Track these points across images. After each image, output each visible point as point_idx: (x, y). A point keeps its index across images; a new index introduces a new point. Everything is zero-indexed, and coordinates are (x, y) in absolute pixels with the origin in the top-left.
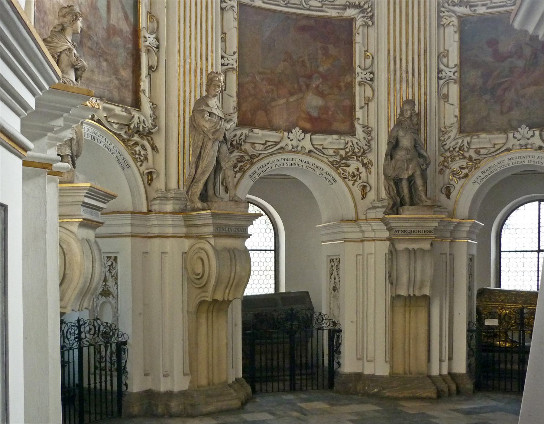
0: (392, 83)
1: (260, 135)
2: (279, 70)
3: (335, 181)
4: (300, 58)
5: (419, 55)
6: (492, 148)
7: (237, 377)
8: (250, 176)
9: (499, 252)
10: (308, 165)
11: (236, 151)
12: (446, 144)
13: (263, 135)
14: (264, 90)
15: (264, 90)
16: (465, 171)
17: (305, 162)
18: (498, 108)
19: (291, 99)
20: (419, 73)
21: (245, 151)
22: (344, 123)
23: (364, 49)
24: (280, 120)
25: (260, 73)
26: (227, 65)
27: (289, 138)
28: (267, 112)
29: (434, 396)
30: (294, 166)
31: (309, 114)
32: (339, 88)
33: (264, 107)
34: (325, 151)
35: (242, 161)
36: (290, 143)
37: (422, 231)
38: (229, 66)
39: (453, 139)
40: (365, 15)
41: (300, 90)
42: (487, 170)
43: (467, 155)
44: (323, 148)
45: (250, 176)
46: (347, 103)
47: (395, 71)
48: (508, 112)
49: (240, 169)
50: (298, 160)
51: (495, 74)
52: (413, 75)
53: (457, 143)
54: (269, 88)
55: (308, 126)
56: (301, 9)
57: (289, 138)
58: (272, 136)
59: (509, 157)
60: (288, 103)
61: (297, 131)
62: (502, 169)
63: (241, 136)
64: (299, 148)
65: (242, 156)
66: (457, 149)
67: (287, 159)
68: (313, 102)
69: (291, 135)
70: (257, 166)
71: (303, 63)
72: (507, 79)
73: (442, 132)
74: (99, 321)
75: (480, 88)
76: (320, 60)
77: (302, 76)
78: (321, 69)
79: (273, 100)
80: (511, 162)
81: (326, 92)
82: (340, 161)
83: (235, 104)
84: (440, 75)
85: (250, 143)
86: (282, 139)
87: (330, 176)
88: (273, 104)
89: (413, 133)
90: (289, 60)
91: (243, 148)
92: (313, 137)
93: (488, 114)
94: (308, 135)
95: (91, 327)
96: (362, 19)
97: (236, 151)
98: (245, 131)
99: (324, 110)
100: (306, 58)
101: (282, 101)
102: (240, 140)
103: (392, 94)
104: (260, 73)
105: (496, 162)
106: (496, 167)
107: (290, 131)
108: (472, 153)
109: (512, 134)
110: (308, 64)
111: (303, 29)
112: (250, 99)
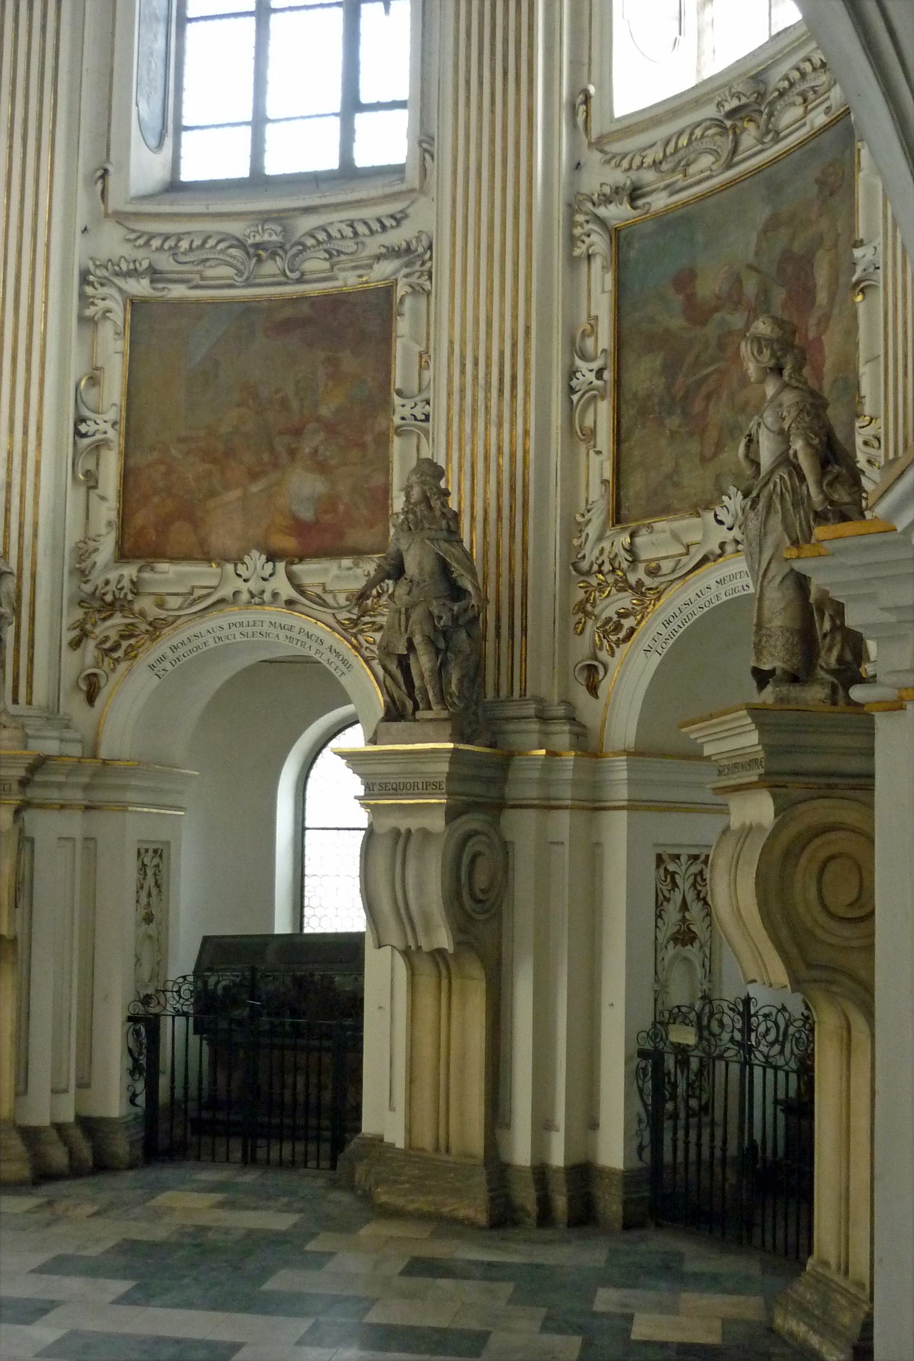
0: (456, 419)
1: (171, 575)
2: (224, 429)
3: (349, 666)
4: (277, 392)
5: (514, 345)
6: (682, 555)
7: (85, 1113)
8: (152, 667)
9: (300, 829)
10: (289, 634)
11: (118, 614)
12: (584, 557)
13: (181, 577)
14: (190, 476)
15: (190, 476)
16: (627, 623)
17: (282, 627)
18: (694, 447)
19: (254, 488)
20: (514, 386)
21: (142, 614)
22: (371, 527)
23: (417, 349)
24: (222, 538)
25: (181, 440)
26: (94, 435)
27: (239, 575)
28: (195, 524)
29: (482, 1218)
30: (258, 638)
31: (295, 518)
32: (363, 446)
33: (190, 513)
34: (329, 598)
35: (131, 636)
36: (244, 587)
37: (420, 786)
38: (99, 436)
39: (602, 544)
40: (417, 267)
41: (275, 465)
42: (674, 616)
43: (632, 579)
44: (325, 591)
45: (152, 667)
46: (377, 480)
47: (462, 390)
48: (715, 455)
49: (126, 653)
50: (266, 625)
51: (690, 358)
52: (501, 391)
53: (602, 551)
54: (201, 469)
55: (289, 543)
56: (285, 284)
57: (239, 575)
58: (201, 574)
59: (717, 576)
60: (245, 498)
61: (256, 560)
62: (706, 609)
63: (119, 582)
64: (267, 596)
65: (132, 624)
66: (607, 567)
67: (241, 624)
68: (303, 488)
69: (241, 569)
70: (169, 644)
71: (284, 404)
72: (712, 368)
73: (573, 528)
74: (787, 1015)
75: (661, 402)
76: (321, 389)
77: (281, 433)
78: (325, 411)
79: (212, 494)
80: (722, 589)
81: (333, 462)
82: (358, 619)
83: (113, 515)
84: (574, 383)
85: (154, 594)
86: (223, 578)
87: (338, 654)
88: (211, 504)
89: (431, 540)
90: (251, 401)
91: (136, 607)
92: (296, 568)
93: (677, 464)
94: (281, 566)
95: (770, 1024)
96: (404, 279)
97: (118, 614)
98: (130, 571)
99: (329, 503)
100: (290, 390)
101: (234, 494)
102: (121, 589)
103: (455, 446)
104: (181, 440)
105: (690, 594)
106: (694, 608)
107: (238, 560)
108: (638, 575)
109: (712, 514)
110: (295, 405)
111: (285, 327)
112: (156, 499)
